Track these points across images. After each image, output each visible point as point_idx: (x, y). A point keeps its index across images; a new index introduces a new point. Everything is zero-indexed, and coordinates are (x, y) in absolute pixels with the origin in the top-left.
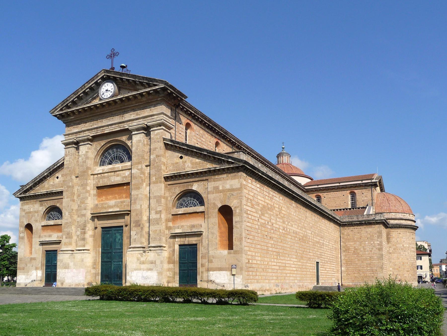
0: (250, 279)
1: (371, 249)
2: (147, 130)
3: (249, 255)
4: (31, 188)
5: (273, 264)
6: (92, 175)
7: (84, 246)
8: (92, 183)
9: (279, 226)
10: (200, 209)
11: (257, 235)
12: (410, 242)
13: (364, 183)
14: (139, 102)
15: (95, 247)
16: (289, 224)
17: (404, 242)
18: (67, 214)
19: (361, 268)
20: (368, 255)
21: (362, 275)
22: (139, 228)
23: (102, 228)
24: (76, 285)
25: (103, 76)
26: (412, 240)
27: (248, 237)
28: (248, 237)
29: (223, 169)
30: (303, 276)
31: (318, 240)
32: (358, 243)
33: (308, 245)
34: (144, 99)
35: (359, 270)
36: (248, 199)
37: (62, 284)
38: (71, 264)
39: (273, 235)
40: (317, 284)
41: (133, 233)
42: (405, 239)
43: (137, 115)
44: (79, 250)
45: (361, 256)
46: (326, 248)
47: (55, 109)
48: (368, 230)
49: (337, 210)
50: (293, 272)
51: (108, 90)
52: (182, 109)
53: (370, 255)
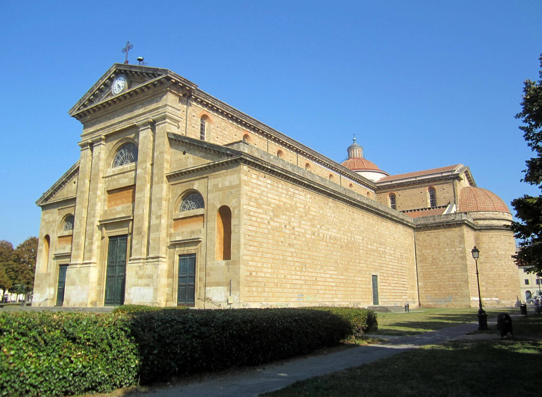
0: (253, 297)
1: (452, 259)
2: (153, 125)
3: (250, 266)
4: (51, 195)
5: (294, 277)
6: (103, 178)
7: (90, 259)
8: (102, 187)
9: (305, 230)
10: (200, 211)
11: (265, 241)
12: (507, 248)
13: (443, 176)
14: (146, 95)
15: (102, 259)
16: (323, 228)
17: (498, 248)
18: (78, 222)
19: (442, 283)
20: (449, 266)
21: (444, 292)
22: (140, 236)
23: (110, 237)
24: (80, 304)
25: (115, 71)
26: (509, 245)
27: (251, 243)
28: (251, 243)
29: (222, 163)
30: (349, 293)
31: (375, 248)
32: (436, 251)
33: (357, 254)
34: (151, 91)
35: (440, 286)
36: (251, 198)
37: (68, 303)
38: (77, 280)
39: (295, 242)
40: (374, 303)
41: (134, 242)
42: (499, 245)
43: (145, 109)
44: (86, 264)
45: (441, 267)
46: (390, 257)
47: (74, 109)
48: (447, 234)
49: (415, 210)
50: (330, 288)
51: (119, 86)
52: (196, 100)
53: (451, 266)
